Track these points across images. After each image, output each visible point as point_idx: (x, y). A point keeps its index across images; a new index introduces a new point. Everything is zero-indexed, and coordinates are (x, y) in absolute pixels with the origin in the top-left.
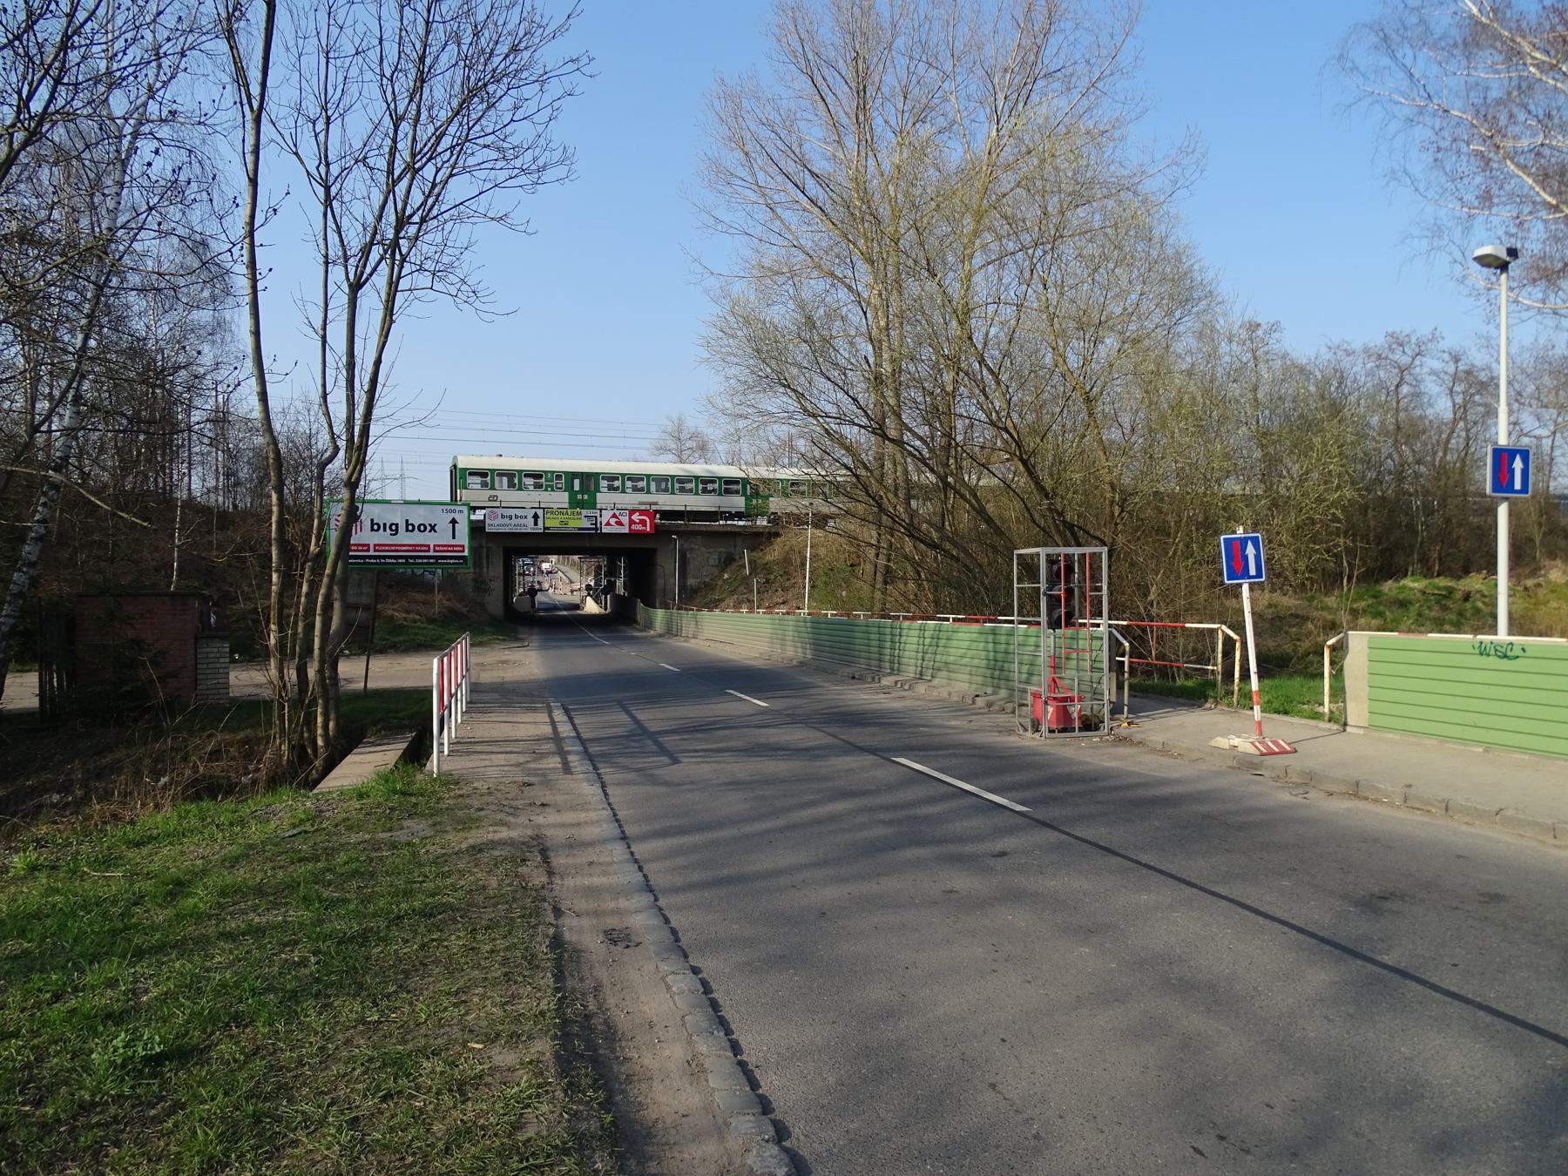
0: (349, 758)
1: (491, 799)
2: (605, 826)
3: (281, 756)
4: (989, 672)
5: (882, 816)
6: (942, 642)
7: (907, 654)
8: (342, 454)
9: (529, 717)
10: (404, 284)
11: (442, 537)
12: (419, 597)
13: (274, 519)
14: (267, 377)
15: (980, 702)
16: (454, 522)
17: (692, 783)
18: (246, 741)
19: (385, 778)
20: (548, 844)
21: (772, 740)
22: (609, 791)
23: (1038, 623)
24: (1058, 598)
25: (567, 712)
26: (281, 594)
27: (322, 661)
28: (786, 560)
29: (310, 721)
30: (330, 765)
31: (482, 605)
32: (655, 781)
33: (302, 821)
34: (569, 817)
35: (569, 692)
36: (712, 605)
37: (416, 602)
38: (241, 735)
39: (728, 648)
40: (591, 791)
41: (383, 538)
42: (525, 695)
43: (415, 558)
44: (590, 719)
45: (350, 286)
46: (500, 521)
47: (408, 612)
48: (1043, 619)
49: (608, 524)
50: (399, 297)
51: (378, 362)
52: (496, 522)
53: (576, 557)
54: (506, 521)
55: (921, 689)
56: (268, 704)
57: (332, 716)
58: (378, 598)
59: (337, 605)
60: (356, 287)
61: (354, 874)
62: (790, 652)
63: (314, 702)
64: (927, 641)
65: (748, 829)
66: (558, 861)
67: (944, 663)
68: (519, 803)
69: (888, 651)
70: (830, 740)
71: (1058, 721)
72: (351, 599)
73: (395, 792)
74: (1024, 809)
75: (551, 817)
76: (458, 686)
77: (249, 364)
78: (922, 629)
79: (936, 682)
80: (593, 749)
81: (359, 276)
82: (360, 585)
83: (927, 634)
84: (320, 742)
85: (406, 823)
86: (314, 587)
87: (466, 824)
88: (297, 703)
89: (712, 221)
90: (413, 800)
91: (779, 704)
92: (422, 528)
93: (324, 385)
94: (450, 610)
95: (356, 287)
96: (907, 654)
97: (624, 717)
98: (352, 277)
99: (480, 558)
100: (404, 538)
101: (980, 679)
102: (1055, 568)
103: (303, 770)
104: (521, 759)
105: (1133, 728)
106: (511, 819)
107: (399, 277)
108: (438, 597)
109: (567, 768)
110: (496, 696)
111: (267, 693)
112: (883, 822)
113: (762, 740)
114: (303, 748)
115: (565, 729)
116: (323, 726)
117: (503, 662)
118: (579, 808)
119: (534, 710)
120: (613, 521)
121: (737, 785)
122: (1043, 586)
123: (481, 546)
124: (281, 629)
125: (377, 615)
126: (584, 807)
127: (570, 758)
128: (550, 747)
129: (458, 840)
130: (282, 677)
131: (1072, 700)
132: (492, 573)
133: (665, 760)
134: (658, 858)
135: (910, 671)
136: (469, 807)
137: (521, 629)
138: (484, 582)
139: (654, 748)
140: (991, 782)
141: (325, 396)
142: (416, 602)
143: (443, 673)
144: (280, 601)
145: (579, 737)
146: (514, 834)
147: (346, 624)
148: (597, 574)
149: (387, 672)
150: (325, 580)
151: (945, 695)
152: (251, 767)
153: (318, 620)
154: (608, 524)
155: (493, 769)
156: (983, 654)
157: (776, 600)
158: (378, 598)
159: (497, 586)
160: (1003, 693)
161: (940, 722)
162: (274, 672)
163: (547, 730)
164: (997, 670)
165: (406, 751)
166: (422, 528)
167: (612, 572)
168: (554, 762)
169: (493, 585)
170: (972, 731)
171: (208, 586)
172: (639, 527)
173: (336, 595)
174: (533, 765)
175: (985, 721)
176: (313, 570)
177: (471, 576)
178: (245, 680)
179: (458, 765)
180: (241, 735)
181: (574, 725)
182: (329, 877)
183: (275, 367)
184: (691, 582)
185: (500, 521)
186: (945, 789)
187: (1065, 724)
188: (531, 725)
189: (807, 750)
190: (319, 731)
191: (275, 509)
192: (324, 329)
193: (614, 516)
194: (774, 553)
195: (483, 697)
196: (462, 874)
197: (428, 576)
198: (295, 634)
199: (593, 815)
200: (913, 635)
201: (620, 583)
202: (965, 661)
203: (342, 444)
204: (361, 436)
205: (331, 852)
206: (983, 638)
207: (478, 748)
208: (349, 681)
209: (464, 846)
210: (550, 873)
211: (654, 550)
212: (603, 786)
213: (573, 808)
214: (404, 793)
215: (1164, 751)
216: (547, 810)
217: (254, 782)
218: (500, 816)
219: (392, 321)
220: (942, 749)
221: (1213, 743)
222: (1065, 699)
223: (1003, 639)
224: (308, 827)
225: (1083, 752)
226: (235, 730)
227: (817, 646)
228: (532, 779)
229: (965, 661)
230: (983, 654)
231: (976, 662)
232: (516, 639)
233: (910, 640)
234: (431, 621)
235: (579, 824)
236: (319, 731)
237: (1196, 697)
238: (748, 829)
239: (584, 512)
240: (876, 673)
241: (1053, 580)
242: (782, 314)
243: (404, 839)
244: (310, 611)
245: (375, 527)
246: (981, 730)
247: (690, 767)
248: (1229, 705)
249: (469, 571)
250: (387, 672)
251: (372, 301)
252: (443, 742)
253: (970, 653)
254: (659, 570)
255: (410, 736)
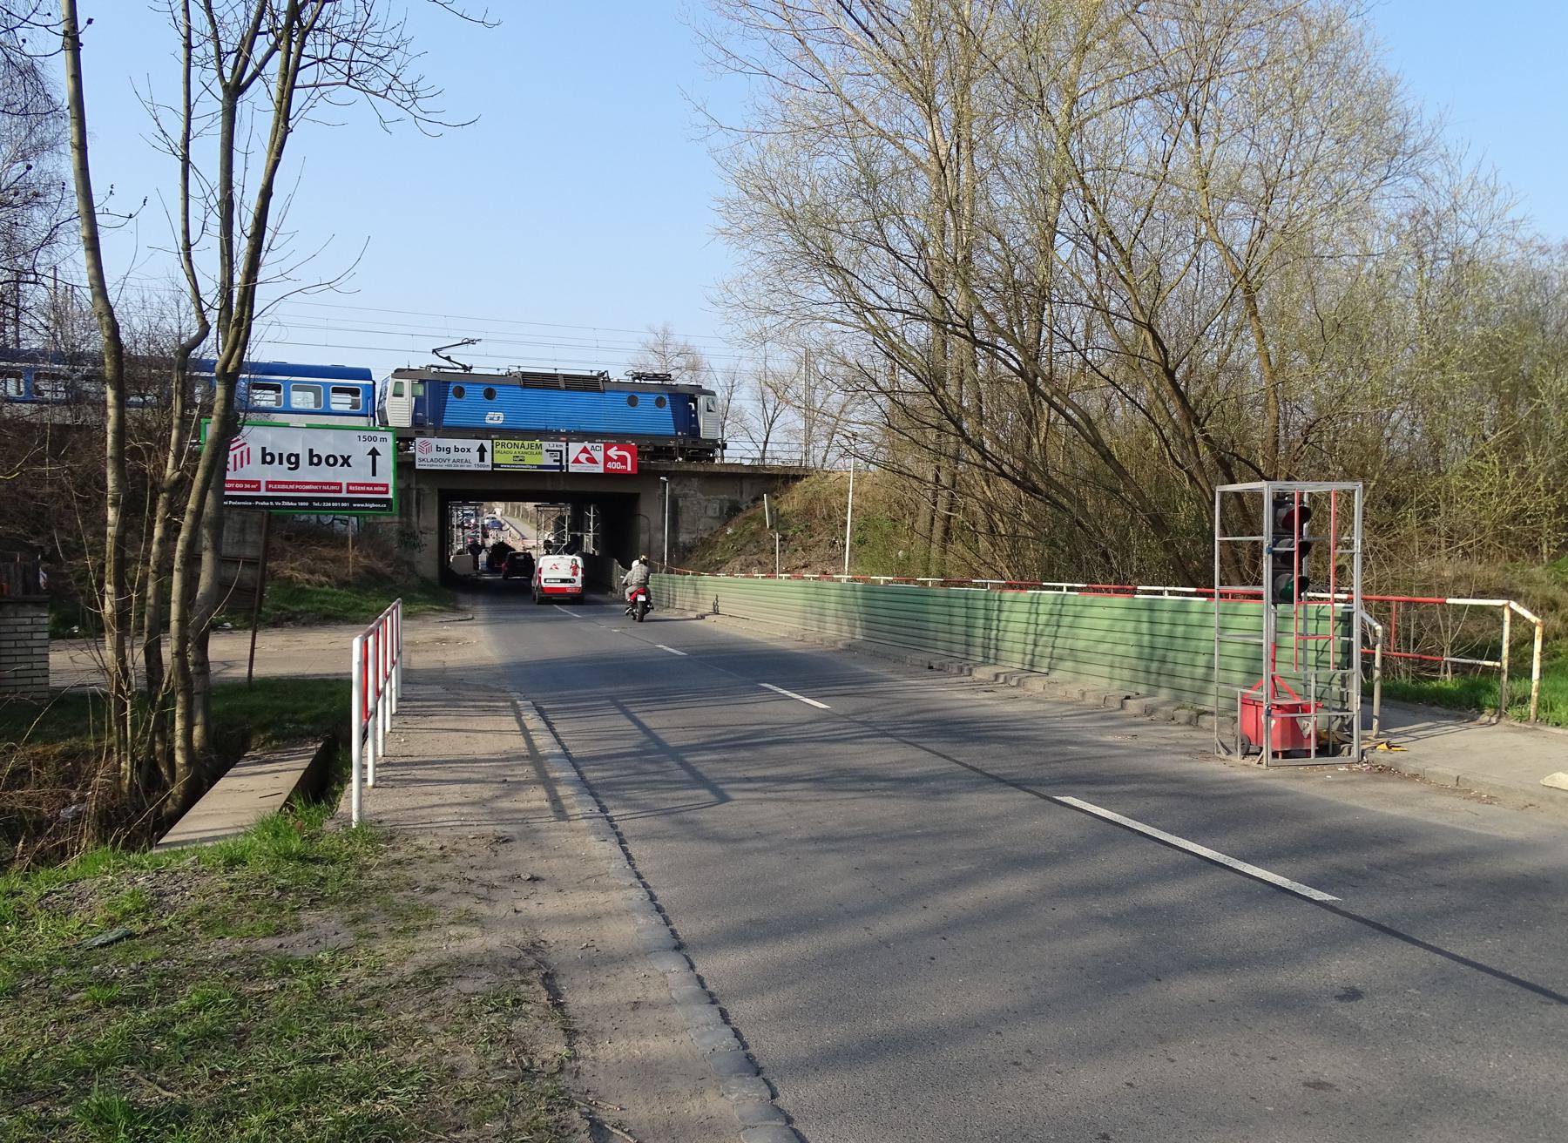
0: (223, 783)
1: (444, 868)
2: (641, 921)
3: (119, 780)
4: (1141, 665)
5: (1098, 906)
6: (1066, 621)
7: (1009, 636)
8: (213, 331)
9: (488, 723)
10: (304, 77)
11: (358, 473)
12: (328, 552)
13: (110, 427)
14: (99, 219)
15: (1133, 706)
16: (374, 453)
17: (760, 836)
18: (69, 755)
19: (272, 828)
20: (553, 960)
21: (860, 762)
22: (633, 850)
23: (1258, 597)
24: (258, 489)
25: (542, 713)
26: (120, 540)
27: (183, 640)
28: (808, 512)
29: (164, 725)
30: (194, 793)
31: (410, 564)
32: (698, 833)
33: (126, 914)
34: (578, 901)
35: (543, 685)
36: (714, 568)
37: (323, 559)
38: (61, 747)
39: (743, 624)
40: (602, 849)
41: (279, 472)
42: (478, 688)
43: (321, 500)
44: (578, 726)
45: (226, 87)
46: (434, 454)
47: (312, 572)
48: (1266, 589)
49: (577, 461)
50: (298, 96)
51: (267, 193)
52: (429, 456)
53: (530, 506)
54: (443, 455)
55: (1036, 685)
56: (99, 700)
57: (199, 719)
58: (269, 553)
59: (207, 558)
60: (234, 91)
61: (209, 1038)
62: (831, 631)
63: (169, 700)
64: (1042, 619)
65: (886, 927)
66: (579, 999)
67: (1069, 650)
68: (493, 875)
69: (980, 632)
70: (940, 765)
71: (1283, 741)
72: (228, 550)
73: (289, 856)
74: (1327, 897)
75: (546, 904)
76: (387, 677)
77: (74, 203)
78: (1035, 602)
79: (1055, 675)
80: (593, 775)
81: (239, 71)
82: (242, 531)
83: (1042, 609)
84: (179, 758)
85: (308, 917)
86: (172, 530)
87: (412, 919)
88: (145, 699)
89: (722, 56)
90: (319, 870)
91: (846, 705)
92: (331, 461)
93: (186, 232)
94: (370, 571)
95: (234, 91)
96: (1009, 636)
97: (624, 723)
98: (227, 73)
99: (409, 503)
100: (306, 474)
101: (1127, 674)
102: (1283, 512)
103: (141, 817)
104: (486, 792)
105: (1396, 754)
106: (483, 909)
107: (297, 69)
108: (351, 553)
109: (560, 812)
110: (438, 689)
111: (98, 683)
112: (1103, 919)
113: (842, 763)
114: (154, 766)
115: (544, 742)
116: (185, 734)
117: (441, 640)
118: (591, 886)
119: (495, 711)
120: (583, 457)
121: (828, 841)
122: (1266, 540)
123: (409, 487)
124: (120, 589)
125: (267, 576)
126: (593, 881)
127: (562, 791)
128: (525, 771)
129: (402, 954)
130: (123, 662)
131: (1306, 709)
132: (423, 523)
133: (705, 794)
134: (748, 990)
135: (1014, 660)
136: (413, 885)
137: (461, 597)
138: (413, 535)
139: (682, 774)
140: (1310, 866)
141: (188, 246)
142: (323, 559)
143: (362, 656)
144: (119, 549)
145: (567, 755)
146: (494, 941)
147: (221, 584)
148: (559, 526)
149: (285, 653)
150: (188, 519)
151: (1076, 695)
152: (74, 795)
153: (177, 578)
154: (577, 461)
155: (443, 811)
156: (1133, 638)
157: (795, 562)
158: (269, 553)
159: (431, 540)
160: (1164, 694)
161: (1089, 737)
162: (109, 654)
163: (517, 743)
164: (1156, 662)
165: (307, 771)
166: (331, 461)
167: (578, 524)
168: (536, 798)
169: (424, 539)
170: (1148, 753)
171: (37, 533)
172: (618, 466)
173: (206, 542)
174: (505, 804)
175: (1151, 736)
176: (170, 504)
177: (395, 527)
178: (71, 664)
179: (390, 803)
180: (61, 747)
181: (556, 735)
182: (159, 1046)
183: (111, 204)
184: (684, 538)
185: (434, 454)
186: (1170, 854)
187: (1293, 748)
188: (493, 735)
189: (916, 780)
190: (178, 742)
191: (111, 412)
192: (187, 147)
193: (585, 450)
194: (793, 501)
195: (427, 692)
196: (408, 1036)
197: (339, 526)
198: (142, 599)
199: (617, 898)
200: (1020, 613)
201: (588, 539)
202: (1102, 647)
203: (212, 317)
204: (242, 304)
205: (169, 984)
206: (1133, 615)
207: (419, 773)
208: (228, 664)
209: (409, 969)
210: (571, 1034)
211: (637, 496)
212: (622, 842)
213: (582, 885)
214: (303, 859)
215: (1460, 787)
216: (541, 887)
217: (78, 817)
218: (465, 903)
219: (287, 130)
220: (1111, 782)
221: (1547, 781)
222: (1294, 708)
223: (1166, 617)
224: (138, 927)
225: (1317, 783)
226: (50, 740)
227: (871, 624)
228: (511, 830)
229: (1102, 647)
230: (1133, 638)
231: (1120, 649)
232: (456, 610)
233: (1014, 616)
234: (343, 584)
235: (596, 917)
236: (178, 742)
237: (1465, 703)
238: (886, 927)
239: (546, 445)
240: (965, 666)
241: (1283, 527)
242: (830, 166)
243: (302, 953)
244: (165, 569)
245: (267, 458)
246: (1157, 750)
247: (748, 810)
248: (1521, 719)
249: (391, 521)
250: (285, 653)
251: (258, 105)
252: (365, 755)
253: (1111, 636)
254: (643, 522)
255: (314, 747)
